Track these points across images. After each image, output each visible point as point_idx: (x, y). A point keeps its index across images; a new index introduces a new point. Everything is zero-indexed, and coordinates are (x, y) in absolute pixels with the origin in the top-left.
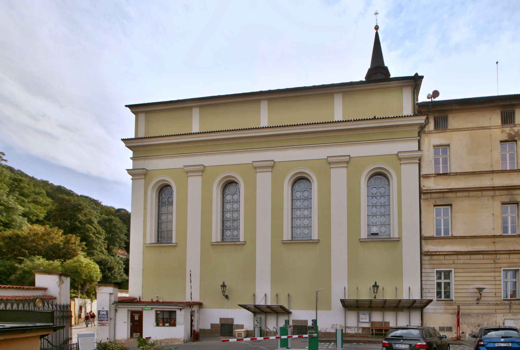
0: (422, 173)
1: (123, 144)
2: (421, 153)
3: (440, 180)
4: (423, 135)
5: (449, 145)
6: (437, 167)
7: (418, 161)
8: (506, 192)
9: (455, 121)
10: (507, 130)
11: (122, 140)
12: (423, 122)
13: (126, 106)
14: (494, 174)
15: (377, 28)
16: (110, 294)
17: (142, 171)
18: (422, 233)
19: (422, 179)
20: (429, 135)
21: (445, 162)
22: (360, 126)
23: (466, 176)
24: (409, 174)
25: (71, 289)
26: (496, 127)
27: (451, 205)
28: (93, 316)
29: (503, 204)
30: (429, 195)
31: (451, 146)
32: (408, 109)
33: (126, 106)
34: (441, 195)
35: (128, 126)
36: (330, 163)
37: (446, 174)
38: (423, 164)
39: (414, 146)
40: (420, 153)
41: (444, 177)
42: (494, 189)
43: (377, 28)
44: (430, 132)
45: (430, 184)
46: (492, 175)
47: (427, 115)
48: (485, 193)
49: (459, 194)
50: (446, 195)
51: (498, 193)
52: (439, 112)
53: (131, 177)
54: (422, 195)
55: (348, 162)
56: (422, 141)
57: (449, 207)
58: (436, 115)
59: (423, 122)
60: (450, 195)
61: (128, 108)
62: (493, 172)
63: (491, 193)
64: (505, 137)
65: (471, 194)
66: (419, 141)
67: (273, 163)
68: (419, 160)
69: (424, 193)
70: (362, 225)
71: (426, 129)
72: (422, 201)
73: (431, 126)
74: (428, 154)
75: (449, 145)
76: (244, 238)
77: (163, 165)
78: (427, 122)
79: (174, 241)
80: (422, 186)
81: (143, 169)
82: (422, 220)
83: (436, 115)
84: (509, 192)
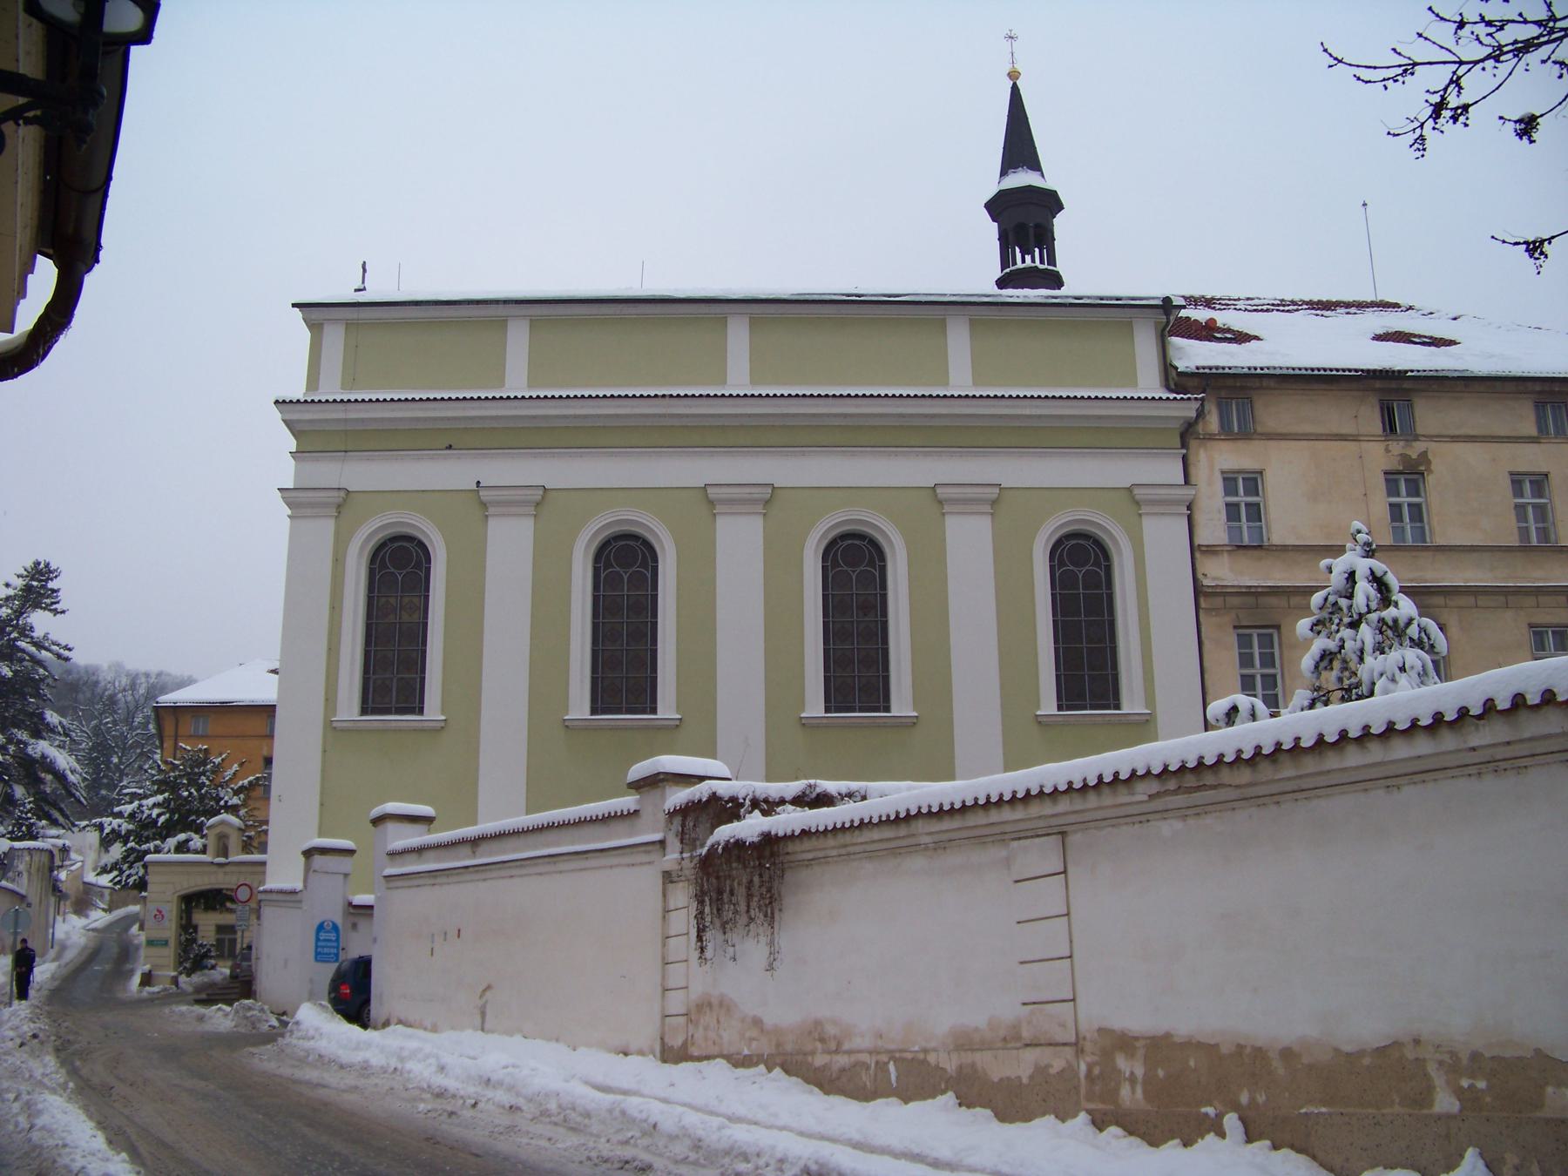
0: (1197, 541)
1: (276, 415)
4: (1193, 443)
6: (1234, 532)
9: (1274, 413)
10: (1397, 447)
12: (1194, 414)
13: (294, 305)
19: (1197, 555)
20: (1210, 444)
21: (1255, 512)
24: (1164, 540)
26: (1371, 438)
27: (1278, 627)
28: (710, 1005)
29: (1393, 429)
30: (1219, 601)
31: (1268, 476)
32: (1149, 384)
33: (294, 305)
37: (1260, 546)
38: (1200, 518)
39: (1174, 472)
40: (1188, 492)
41: (1256, 553)
44: (1211, 437)
45: (1221, 572)
52: (1237, 394)
53: (289, 512)
54: (1202, 600)
55: (994, 503)
56: (1191, 459)
60: (1273, 601)
64: (1395, 465)
68: (1189, 508)
69: (1207, 595)
70: (674, 648)
71: (1200, 428)
73: (1213, 422)
74: (1212, 500)
78: (1201, 414)
80: (1200, 576)
82: (1206, 664)
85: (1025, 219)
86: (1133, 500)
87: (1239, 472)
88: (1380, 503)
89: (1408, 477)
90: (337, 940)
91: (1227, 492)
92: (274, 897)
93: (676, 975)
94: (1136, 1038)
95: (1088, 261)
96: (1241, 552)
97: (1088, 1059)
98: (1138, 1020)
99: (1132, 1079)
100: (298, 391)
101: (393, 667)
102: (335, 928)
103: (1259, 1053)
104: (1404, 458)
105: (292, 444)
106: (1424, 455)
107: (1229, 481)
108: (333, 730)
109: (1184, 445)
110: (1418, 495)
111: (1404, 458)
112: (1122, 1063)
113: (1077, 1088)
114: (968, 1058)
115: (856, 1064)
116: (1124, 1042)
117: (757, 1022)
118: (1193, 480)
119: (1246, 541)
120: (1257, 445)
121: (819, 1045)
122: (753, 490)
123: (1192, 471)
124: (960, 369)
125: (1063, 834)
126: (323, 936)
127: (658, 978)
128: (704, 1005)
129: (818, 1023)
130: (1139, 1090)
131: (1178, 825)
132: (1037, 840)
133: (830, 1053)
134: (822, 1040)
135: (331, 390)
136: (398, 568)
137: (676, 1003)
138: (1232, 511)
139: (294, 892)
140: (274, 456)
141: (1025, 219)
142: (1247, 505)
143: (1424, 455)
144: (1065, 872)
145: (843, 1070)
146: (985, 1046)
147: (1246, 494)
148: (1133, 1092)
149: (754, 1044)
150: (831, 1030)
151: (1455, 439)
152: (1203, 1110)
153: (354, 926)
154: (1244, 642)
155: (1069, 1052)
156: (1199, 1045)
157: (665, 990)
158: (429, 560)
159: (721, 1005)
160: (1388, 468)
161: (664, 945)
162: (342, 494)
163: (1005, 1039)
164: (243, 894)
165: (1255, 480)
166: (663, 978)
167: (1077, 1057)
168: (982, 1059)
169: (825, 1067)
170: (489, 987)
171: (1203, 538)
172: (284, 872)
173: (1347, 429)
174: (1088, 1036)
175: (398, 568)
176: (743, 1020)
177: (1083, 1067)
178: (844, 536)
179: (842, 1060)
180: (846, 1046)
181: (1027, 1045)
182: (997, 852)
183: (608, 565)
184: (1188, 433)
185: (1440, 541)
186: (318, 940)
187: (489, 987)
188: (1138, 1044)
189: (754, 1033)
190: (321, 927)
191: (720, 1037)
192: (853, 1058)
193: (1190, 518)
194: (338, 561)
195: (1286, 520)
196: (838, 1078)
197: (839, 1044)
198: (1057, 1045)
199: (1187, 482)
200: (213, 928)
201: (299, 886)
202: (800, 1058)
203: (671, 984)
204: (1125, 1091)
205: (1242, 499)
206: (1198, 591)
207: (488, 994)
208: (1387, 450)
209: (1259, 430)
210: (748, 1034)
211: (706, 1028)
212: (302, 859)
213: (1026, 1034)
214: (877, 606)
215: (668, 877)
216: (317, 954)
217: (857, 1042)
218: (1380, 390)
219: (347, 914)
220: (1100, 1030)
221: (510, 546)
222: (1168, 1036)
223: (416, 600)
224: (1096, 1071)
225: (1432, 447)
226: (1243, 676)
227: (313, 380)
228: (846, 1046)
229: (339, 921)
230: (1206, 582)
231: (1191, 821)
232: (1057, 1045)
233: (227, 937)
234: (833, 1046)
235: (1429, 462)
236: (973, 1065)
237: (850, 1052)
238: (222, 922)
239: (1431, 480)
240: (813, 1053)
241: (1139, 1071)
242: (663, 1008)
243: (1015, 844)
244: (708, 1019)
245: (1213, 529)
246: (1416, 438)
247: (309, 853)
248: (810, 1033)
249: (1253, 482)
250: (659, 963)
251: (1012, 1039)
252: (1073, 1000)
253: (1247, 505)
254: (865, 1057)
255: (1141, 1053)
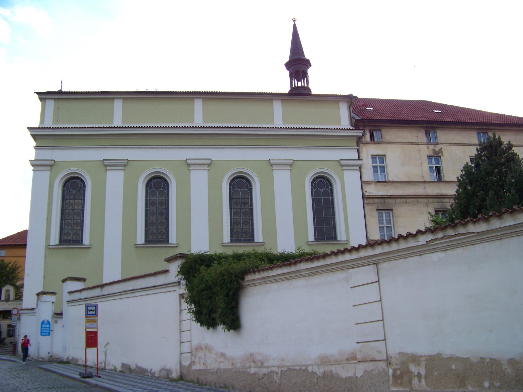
0: (363, 180)
1: (28, 133)
2: (361, 162)
3: (379, 186)
4: (361, 145)
5: (385, 156)
7: (358, 168)
8: (436, 200)
10: (431, 147)
11: (28, 128)
12: (361, 135)
14: (426, 184)
15: (294, 21)
16: (53, 302)
17: (50, 162)
18: (368, 236)
20: (367, 145)
21: (383, 170)
22: (305, 133)
23: (402, 185)
25: (490, 358)
26: (422, 144)
27: (392, 210)
28: (201, 348)
30: (371, 200)
31: (387, 156)
32: (345, 122)
34: (382, 200)
35: (33, 114)
36: (272, 165)
38: (364, 171)
40: (359, 162)
41: (384, 184)
42: (427, 197)
43: (294, 21)
44: (367, 143)
45: (372, 190)
46: (423, 184)
47: (364, 130)
48: (419, 200)
49: (398, 200)
50: (387, 200)
51: (430, 200)
53: (33, 169)
54: (365, 201)
56: (361, 151)
57: (391, 212)
58: (371, 128)
59: (361, 135)
60: (390, 201)
61: (36, 94)
62: (424, 182)
63: (425, 200)
65: (408, 200)
66: (358, 150)
67: (210, 161)
68: (360, 168)
71: (363, 140)
72: (365, 205)
73: (368, 137)
75: (385, 156)
76: (90, 242)
77: (75, 158)
78: (364, 134)
79: (86, 240)
80: (364, 192)
81: (51, 160)
83: (371, 128)
84: (440, 200)
85: (298, 65)
86: (341, 164)
87: (377, 155)
88: (426, 167)
89: (436, 156)
90: (49, 327)
91: (373, 163)
92: (25, 311)
93: (186, 336)
94: (421, 357)
95: (318, 83)
96: (378, 184)
97: (393, 367)
98: (423, 348)
99: (419, 376)
100: (36, 124)
101: (71, 231)
102: (49, 323)
103: (494, 362)
104: (434, 151)
105: (34, 144)
106: (441, 149)
107: (374, 157)
108: (49, 248)
109: (358, 146)
110: (438, 164)
111: (434, 151)
112: (413, 368)
113: (388, 381)
114: (328, 368)
115: (271, 372)
116: (415, 359)
117: (223, 355)
118: (361, 158)
119: (380, 180)
120: (383, 146)
121: (252, 364)
122: (204, 161)
123: (361, 155)
124: (278, 117)
125: (377, 264)
126: (44, 326)
127: (179, 339)
128: (199, 348)
129: (252, 355)
130: (423, 381)
131: (441, 255)
132: (363, 268)
133: (258, 367)
134: (254, 362)
135: (49, 123)
136: (74, 187)
137: (186, 348)
138: (375, 168)
139: (33, 309)
140: (28, 148)
141: (298, 65)
142: (380, 167)
143: (441, 149)
144: (378, 281)
145: (265, 375)
146: (337, 362)
147: (380, 163)
148: (420, 381)
149: (222, 364)
150: (258, 358)
151: (451, 144)
152: (429, 389)
153: (56, 322)
154: (380, 216)
155: (383, 365)
156: (458, 359)
157: (181, 343)
158: (85, 186)
159: (206, 348)
160: (429, 154)
161: (180, 324)
162: (53, 162)
163: (347, 359)
164: (15, 312)
165: (383, 158)
166: (180, 338)
167: (387, 366)
168: (337, 369)
169: (255, 374)
170: (108, 343)
171: (365, 178)
172: (29, 299)
173: (414, 141)
174: (393, 356)
175: (74, 187)
176: (216, 354)
177: (391, 371)
178: (237, 178)
179: (264, 371)
180: (266, 364)
181: (359, 361)
182: (340, 275)
183: (151, 188)
184: (359, 140)
185: (447, 179)
186: (42, 327)
187: (108, 343)
188: (421, 359)
189: (222, 359)
190: (43, 323)
191: (206, 361)
192: (269, 370)
193: (360, 171)
194: (51, 187)
195: (396, 170)
196: (262, 378)
197: (262, 363)
198: (376, 361)
199: (359, 158)
200: (6, 326)
201: (35, 307)
202: (244, 370)
203: (184, 340)
204: (415, 381)
205: (378, 164)
206: (364, 197)
207: (108, 346)
208: (428, 148)
209: (384, 141)
210: (219, 360)
211: (199, 358)
212: (36, 297)
213: (359, 356)
214: (249, 203)
215: (181, 295)
216: (41, 332)
217: (271, 363)
218: (426, 127)
219: (53, 317)
220: (399, 353)
221: (115, 180)
222: (439, 355)
223: (80, 201)
224: (398, 372)
225: (444, 147)
226: (380, 227)
227: (42, 120)
228: (266, 364)
229: (50, 320)
230: (366, 194)
231: (449, 252)
232: (376, 361)
233: (11, 329)
234: (259, 364)
235: (442, 152)
236: (331, 371)
237: (268, 367)
238: (10, 324)
239: (443, 158)
240: (250, 367)
241: (423, 372)
242: (180, 351)
243: (351, 270)
244: (201, 354)
245: (368, 175)
246: (438, 144)
247: (38, 295)
248: (248, 359)
249: (382, 158)
250: (179, 332)
251: (352, 358)
252: (385, 340)
253: (380, 167)
254: (275, 369)
255: (423, 364)
